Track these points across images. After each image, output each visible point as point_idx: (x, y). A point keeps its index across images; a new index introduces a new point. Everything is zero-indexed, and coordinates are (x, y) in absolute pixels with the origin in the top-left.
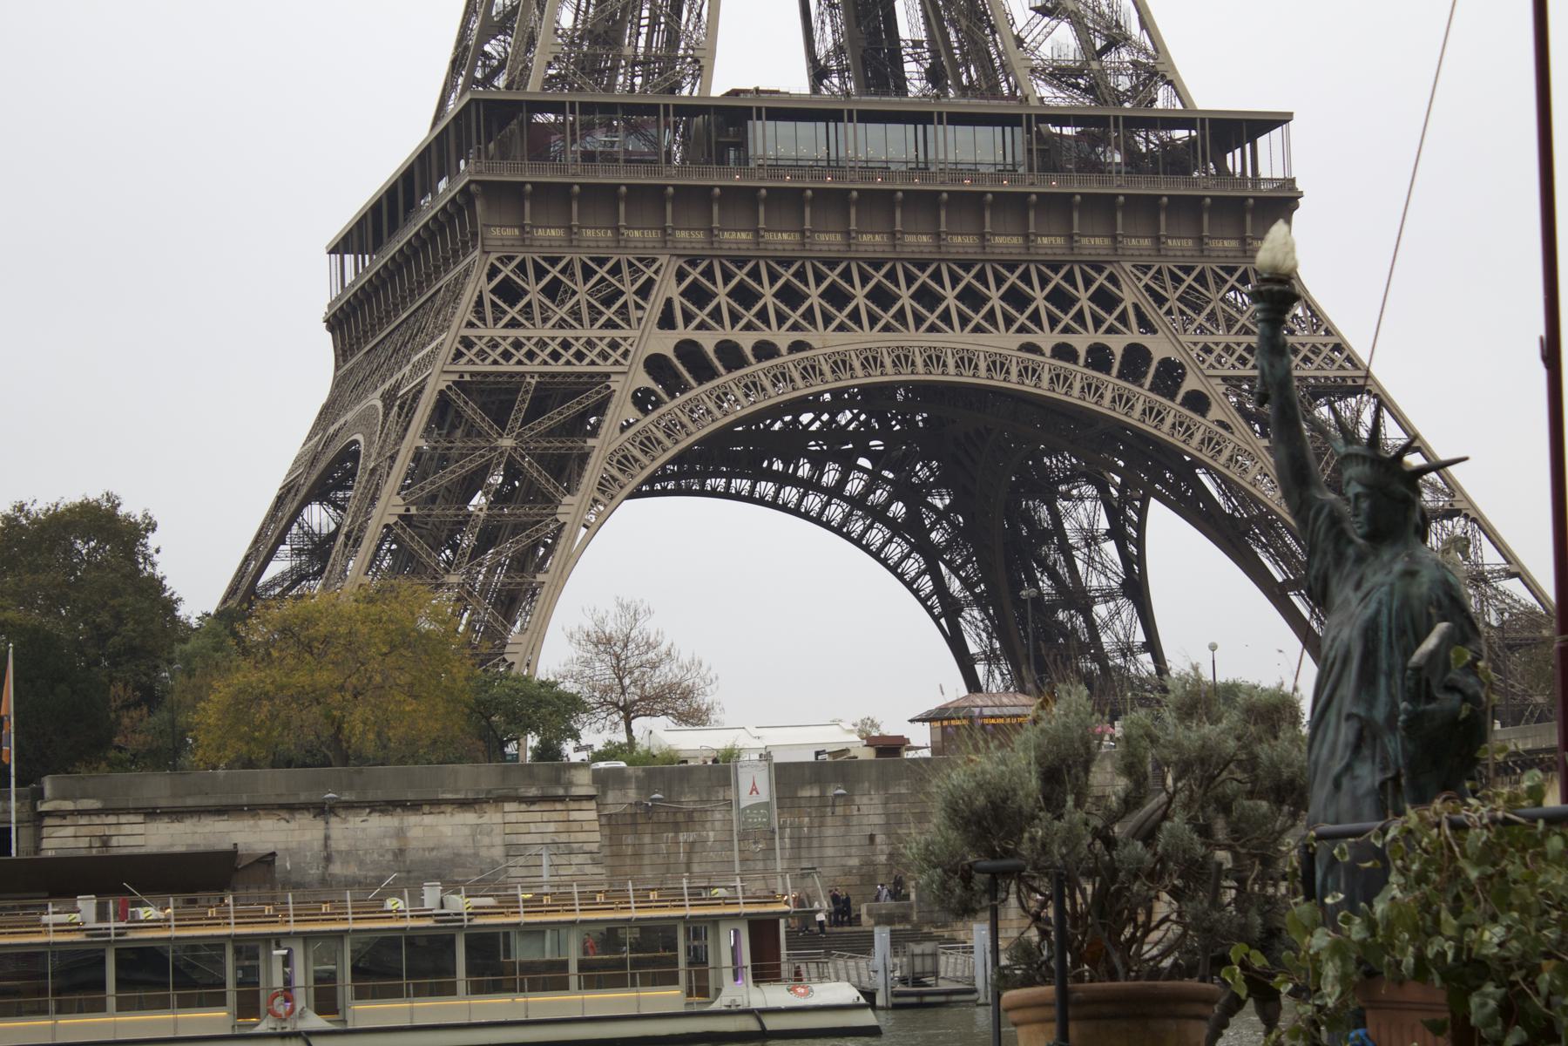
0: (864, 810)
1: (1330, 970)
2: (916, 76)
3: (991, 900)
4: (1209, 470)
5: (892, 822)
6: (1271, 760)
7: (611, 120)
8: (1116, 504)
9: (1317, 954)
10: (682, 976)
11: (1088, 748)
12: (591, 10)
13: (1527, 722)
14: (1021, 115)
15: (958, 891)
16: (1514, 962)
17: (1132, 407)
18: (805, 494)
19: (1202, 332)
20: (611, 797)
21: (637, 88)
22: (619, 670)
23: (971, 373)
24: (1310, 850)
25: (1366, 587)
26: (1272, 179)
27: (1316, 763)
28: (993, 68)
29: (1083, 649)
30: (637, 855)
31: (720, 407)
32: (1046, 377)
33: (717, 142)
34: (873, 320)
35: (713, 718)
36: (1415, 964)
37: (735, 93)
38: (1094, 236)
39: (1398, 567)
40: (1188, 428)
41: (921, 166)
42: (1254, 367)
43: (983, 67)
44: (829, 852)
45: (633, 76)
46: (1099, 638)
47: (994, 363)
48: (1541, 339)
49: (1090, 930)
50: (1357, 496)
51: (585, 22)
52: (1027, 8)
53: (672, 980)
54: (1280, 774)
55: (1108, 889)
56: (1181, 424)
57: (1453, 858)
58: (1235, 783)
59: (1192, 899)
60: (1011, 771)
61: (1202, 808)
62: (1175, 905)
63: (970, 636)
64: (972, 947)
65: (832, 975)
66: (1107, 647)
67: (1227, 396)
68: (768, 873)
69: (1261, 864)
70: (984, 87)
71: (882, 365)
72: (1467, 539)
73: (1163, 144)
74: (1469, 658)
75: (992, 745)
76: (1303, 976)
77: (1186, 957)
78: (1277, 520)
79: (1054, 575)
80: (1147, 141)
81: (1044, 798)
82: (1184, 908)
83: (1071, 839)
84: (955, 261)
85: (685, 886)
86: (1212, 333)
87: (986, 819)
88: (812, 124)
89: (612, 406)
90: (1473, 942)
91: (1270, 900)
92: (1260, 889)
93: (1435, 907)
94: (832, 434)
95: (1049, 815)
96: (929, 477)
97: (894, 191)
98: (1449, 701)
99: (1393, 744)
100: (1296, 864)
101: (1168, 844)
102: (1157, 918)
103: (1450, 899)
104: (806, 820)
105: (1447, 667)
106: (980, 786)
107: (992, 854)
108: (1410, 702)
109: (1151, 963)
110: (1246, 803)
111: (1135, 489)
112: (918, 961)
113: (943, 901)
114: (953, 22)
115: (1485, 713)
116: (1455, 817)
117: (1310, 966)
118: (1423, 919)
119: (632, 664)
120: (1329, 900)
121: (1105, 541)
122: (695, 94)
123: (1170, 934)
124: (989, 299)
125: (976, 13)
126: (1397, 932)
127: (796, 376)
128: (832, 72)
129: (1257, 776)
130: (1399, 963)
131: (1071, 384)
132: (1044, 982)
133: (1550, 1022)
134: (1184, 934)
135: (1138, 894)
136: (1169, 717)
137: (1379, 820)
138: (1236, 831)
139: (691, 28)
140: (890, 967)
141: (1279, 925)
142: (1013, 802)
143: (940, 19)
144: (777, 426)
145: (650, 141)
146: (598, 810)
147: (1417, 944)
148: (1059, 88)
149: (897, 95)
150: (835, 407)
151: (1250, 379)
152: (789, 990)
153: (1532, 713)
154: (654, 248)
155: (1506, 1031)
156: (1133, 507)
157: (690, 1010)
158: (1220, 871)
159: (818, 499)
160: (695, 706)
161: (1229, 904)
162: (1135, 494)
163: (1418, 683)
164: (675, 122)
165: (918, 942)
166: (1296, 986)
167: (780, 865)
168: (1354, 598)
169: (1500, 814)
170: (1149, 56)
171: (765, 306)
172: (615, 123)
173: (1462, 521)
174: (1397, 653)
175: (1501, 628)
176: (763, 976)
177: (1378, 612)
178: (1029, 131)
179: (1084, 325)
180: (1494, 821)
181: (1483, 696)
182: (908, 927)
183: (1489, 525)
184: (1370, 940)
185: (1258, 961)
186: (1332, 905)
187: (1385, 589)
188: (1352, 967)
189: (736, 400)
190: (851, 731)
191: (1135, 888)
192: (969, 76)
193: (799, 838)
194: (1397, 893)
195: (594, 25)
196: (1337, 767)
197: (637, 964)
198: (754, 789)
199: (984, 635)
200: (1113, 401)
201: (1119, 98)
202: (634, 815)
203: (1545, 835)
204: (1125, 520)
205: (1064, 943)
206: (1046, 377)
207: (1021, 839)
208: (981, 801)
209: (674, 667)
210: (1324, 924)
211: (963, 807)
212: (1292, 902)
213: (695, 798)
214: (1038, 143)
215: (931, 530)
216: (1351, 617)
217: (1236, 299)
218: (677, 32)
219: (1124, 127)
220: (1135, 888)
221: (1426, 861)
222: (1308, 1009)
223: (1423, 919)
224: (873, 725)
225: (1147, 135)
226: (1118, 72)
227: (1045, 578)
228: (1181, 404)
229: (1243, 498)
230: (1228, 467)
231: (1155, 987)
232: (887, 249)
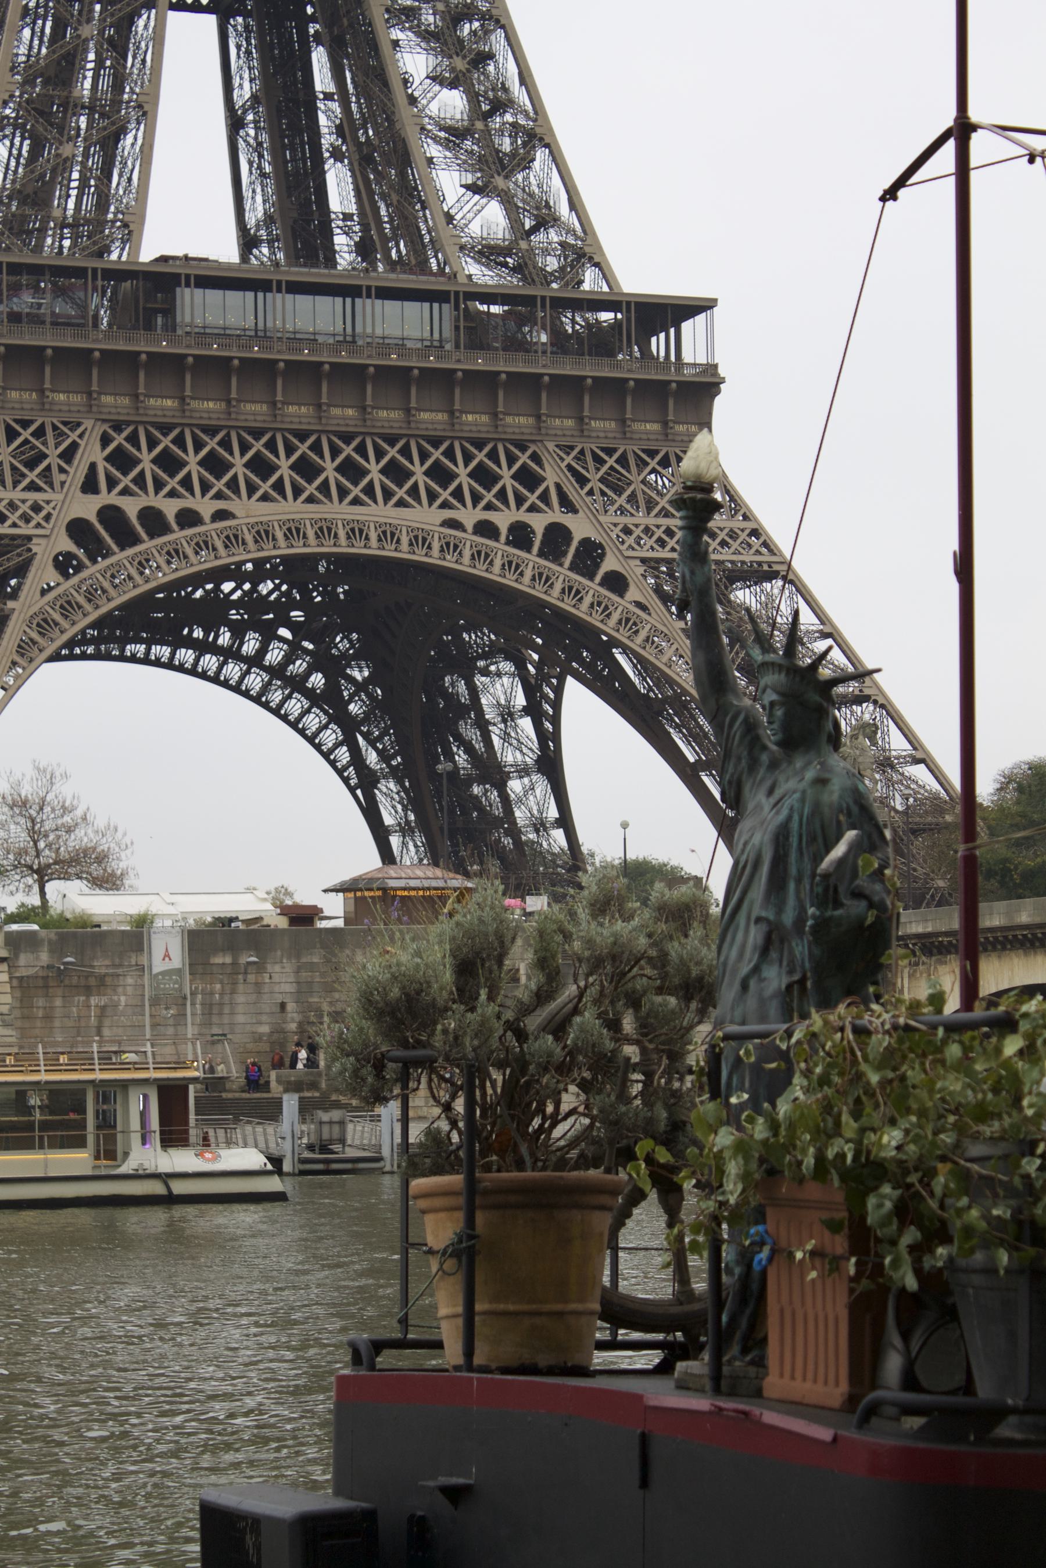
0: (276, 978)
1: (733, 1168)
2: (346, 249)
3: (402, 1089)
4: (626, 650)
5: (303, 990)
6: (681, 959)
7: (39, 282)
8: (533, 681)
9: (721, 1151)
10: (90, 1139)
11: (502, 942)
12: (20, 170)
13: (928, 906)
14: (449, 292)
15: (370, 1080)
16: (910, 1165)
17: (551, 586)
18: (225, 663)
19: (622, 513)
20: (23, 959)
21: (65, 251)
22: (34, 832)
24: (717, 1050)
25: (778, 793)
26: (695, 364)
27: (725, 964)
28: (423, 243)
29: (497, 822)
30: (48, 1017)
31: (142, 573)
32: (467, 553)
33: (144, 308)
34: (297, 491)
35: (127, 882)
36: (816, 1164)
37: (164, 259)
38: (519, 415)
39: (810, 775)
40: (606, 608)
41: (349, 339)
42: (673, 550)
43: (412, 242)
44: (240, 1019)
45: (62, 238)
46: (513, 813)
47: (416, 537)
48: (955, 553)
49: (499, 1120)
50: (772, 704)
51: (14, 182)
52: (458, 185)
53: (79, 1143)
54: (689, 971)
55: (518, 1081)
56: (599, 604)
57: (855, 1062)
58: (645, 979)
59: (600, 1092)
60: (426, 965)
62: (583, 1097)
63: (386, 808)
64: (379, 1116)
65: (240, 1141)
66: (520, 822)
67: (644, 577)
68: (178, 1040)
69: (668, 1058)
70: (413, 262)
71: (305, 537)
72: (875, 725)
73: (589, 326)
74: (876, 865)
75: (407, 937)
76: (706, 1172)
77: (592, 1148)
78: (690, 702)
79: (469, 749)
80: (574, 322)
81: (458, 990)
82: (592, 1100)
83: (483, 1031)
84: (380, 436)
85: (95, 1049)
86: (632, 515)
87: (399, 1010)
88: (240, 294)
89: (33, 570)
90: (873, 1144)
91: (676, 1094)
92: (666, 1083)
93: (836, 1109)
94: (254, 604)
95: (463, 1007)
96: (348, 650)
97: (321, 364)
98: (855, 908)
99: (800, 948)
100: (702, 1063)
101: (578, 1039)
102: (565, 1108)
103: (850, 1101)
104: (218, 986)
105: (855, 875)
106: (394, 977)
107: (405, 1045)
108: (818, 908)
109: (558, 1153)
110: (659, 999)
111: (552, 666)
112: (326, 1129)
113: (355, 1089)
114: (384, 197)
115: (890, 919)
116: (858, 1022)
117: (713, 1163)
118: (824, 1120)
119: (47, 828)
120: (733, 1100)
121: (521, 717)
122: (124, 258)
123: (577, 1126)
124: (412, 474)
125: (407, 188)
126: (799, 1133)
127: (219, 544)
128: (261, 241)
129: (667, 974)
130: (800, 1163)
131: (492, 561)
132: (452, 1171)
133: (943, 1223)
134: (591, 1126)
135: (547, 1086)
136: (583, 914)
137: (785, 1022)
138: (644, 1026)
139: (121, 192)
140: (298, 1134)
141: (684, 1118)
142: (427, 994)
143: (371, 193)
144: (199, 594)
145: (77, 304)
146: (10, 972)
147: (818, 1145)
148: (487, 266)
149: (326, 267)
150: (256, 578)
151: (668, 562)
152: (196, 1155)
153: (933, 896)
154: (79, 411)
155: (901, 1231)
156: (550, 685)
157: (97, 1173)
158: (629, 1066)
159: (237, 668)
160: (109, 870)
161: (636, 1097)
162: (553, 672)
163: (826, 890)
164: (103, 286)
165: (326, 1110)
167: (190, 1031)
168: (767, 804)
169: (902, 1021)
170: (577, 238)
171: (189, 474)
172: (42, 285)
173: (871, 707)
174: (806, 859)
175: (905, 813)
176: (171, 1140)
177: (789, 818)
178: (457, 308)
179: (506, 502)
180: (895, 1027)
181: (889, 903)
182: (317, 1094)
183: (897, 712)
184: (772, 1140)
185: (663, 1156)
186: (736, 1105)
187: (797, 796)
188: (754, 1166)
189: (158, 567)
190: (265, 900)
191: (545, 1080)
192: (399, 251)
193: (211, 1005)
194: (799, 1094)
195: (22, 185)
196: (745, 969)
197: (45, 1126)
198: (167, 955)
199: (399, 807)
200: (533, 579)
201: (546, 278)
202: (45, 978)
203: (945, 1042)
204: (541, 697)
205: (472, 1132)
206: (467, 553)
207: (434, 1031)
208: (395, 992)
209: (90, 831)
210: (728, 1123)
211: (378, 998)
212: (697, 1100)
213: (107, 962)
214: (465, 320)
215: (350, 701)
217: (656, 482)
218: (107, 196)
219: (551, 308)
220: (545, 1080)
221: (829, 1065)
222: (710, 1205)
223: (824, 1120)
224: (288, 893)
225: (573, 316)
226: (546, 252)
227: (461, 753)
228: (599, 584)
229: (658, 678)
230: (644, 648)
231: (561, 1178)
232: (312, 421)
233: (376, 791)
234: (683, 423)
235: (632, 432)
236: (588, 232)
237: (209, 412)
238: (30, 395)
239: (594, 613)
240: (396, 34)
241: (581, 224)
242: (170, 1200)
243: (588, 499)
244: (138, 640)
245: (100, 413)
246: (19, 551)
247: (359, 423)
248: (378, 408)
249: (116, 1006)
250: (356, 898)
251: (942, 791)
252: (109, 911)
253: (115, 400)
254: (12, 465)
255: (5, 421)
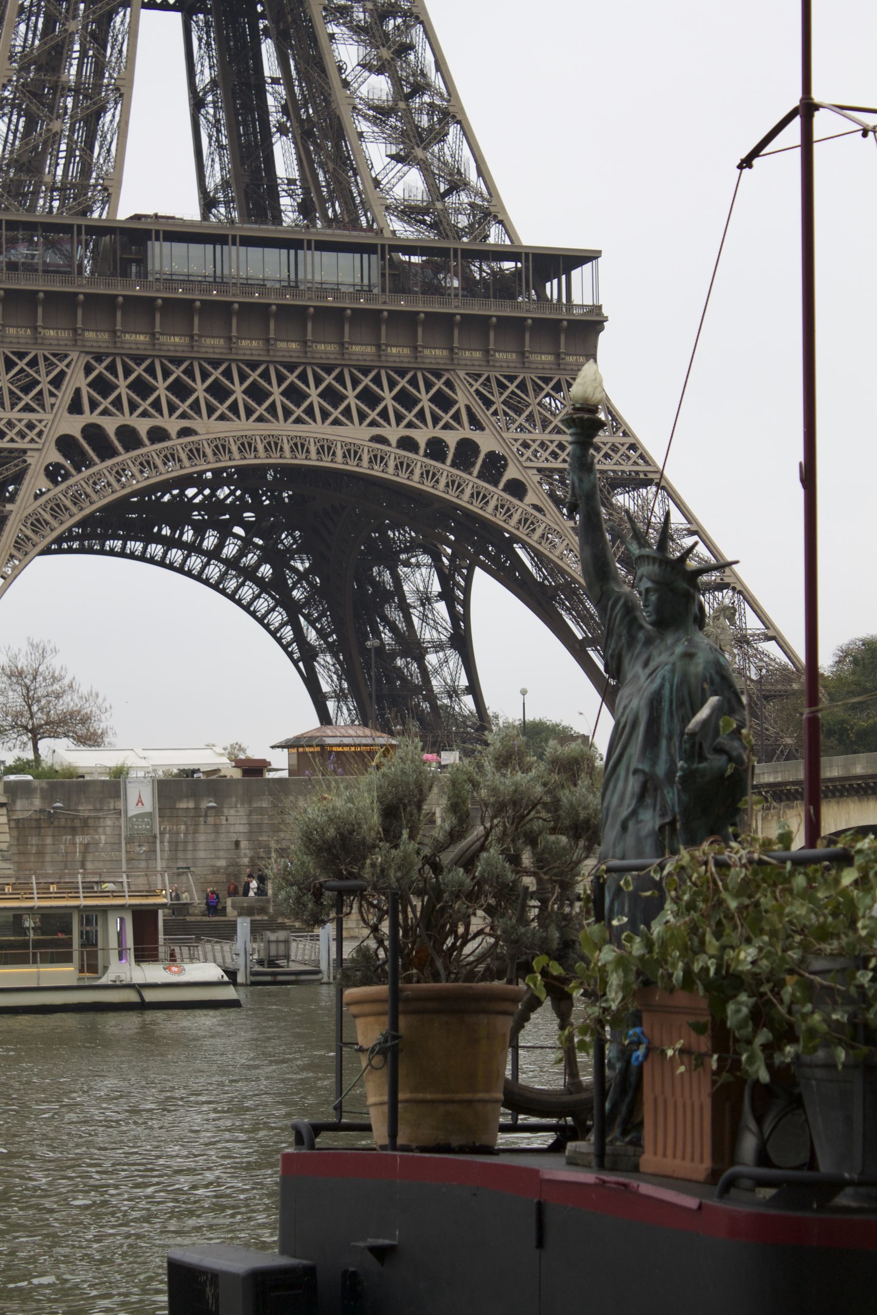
0: (232, 820)
1: (614, 980)
2: (290, 209)
3: (337, 914)
4: (525, 545)
5: (254, 830)
6: (571, 804)
7: (33, 236)
8: (447, 571)
9: (604, 966)
10: (76, 956)
11: (421, 790)
12: (17, 143)
13: (778, 759)
14: (376, 245)
15: (310, 905)
16: (763, 977)
17: (462, 491)
18: (189, 556)
19: (521, 430)
20: (20, 804)
21: (55, 210)
22: (29, 698)
23: (278, 454)
24: (601, 881)
25: (652, 665)
26: (583, 306)
27: (608, 808)
28: (354, 204)
29: (417, 689)
30: (41, 853)
31: (119, 481)
32: (392, 464)
33: (121, 259)
34: (249, 412)
35: (106, 740)
36: (684, 976)
37: (137, 217)
38: (435, 348)
39: (679, 650)
40: (508, 510)
41: (292, 284)
42: (564, 461)
43: (346, 203)
44: (202, 854)
45: (52, 200)
46: (430, 682)
47: (349, 451)
48: (800, 464)
49: (418, 940)
51: (11, 152)
52: (384, 155)
53: (66, 958)
54: (578, 814)
55: (434, 906)
56: (502, 507)
57: (717, 890)
58: (540, 821)
59: (503, 915)
60: (357, 809)
61: (513, 841)
62: (489, 920)
63: (323, 678)
64: (318, 936)
65: (201, 957)
66: (436, 690)
67: (540, 484)
68: (149, 872)
69: (560, 887)
70: (347, 220)
71: (256, 450)
72: (734, 608)
73: (494, 273)
74: (735, 726)
78: (579, 588)
79: (393, 628)
80: (481, 270)
81: (384, 830)
82: (496, 923)
83: (405, 865)
84: (319, 365)
85: (80, 880)
86: (530, 432)
87: (335, 847)
88: (201, 246)
89: (28, 478)
90: (732, 960)
91: (567, 918)
92: (559, 908)
93: (701, 930)
94: (213, 506)
95: (388, 845)
96: (292, 545)
97: (269, 305)
98: (717, 761)
99: (671, 795)
100: (589, 892)
101: (484, 871)
102: (473, 929)
103: (713, 923)
104: (183, 827)
105: (717, 733)
106: (331, 820)
107: (339, 876)
108: (686, 762)
110: (552, 838)
111: (463, 559)
112: (273, 947)
113: (297, 913)
114: (322, 165)
115: (746, 770)
116: (719, 857)
117: (598, 975)
118: (691, 939)
119: (40, 694)
120: (615, 923)
121: (437, 601)
122: (104, 217)
123: (484, 944)
124: (346, 397)
125: (341, 157)
126: (670, 950)
127: (184, 456)
128: (219, 202)
129: (559, 817)
130: (670, 976)
131: (412, 470)
132: (379, 982)
133: (791, 1026)
134: (496, 944)
135: (459, 911)
136: (489, 767)
137: (658, 857)
138: (540, 861)
139: (101, 161)
140: (250, 951)
141: (573, 938)
142: (358, 834)
143: (311, 162)
144: (167, 498)
145: (64, 255)
146: (8, 816)
147: (686, 960)
148: (408, 223)
149: (273, 224)
150: (215, 485)
151: (560, 471)
152: (165, 969)
153: (782, 751)
154: (66, 345)
156: (461, 574)
157: (81, 983)
158: (527, 894)
159: (199, 560)
160: (92, 730)
161: (533, 920)
162: (464, 564)
163: (693, 746)
164: (86, 240)
165: (273, 930)
166: (586, 991)
167: (160, 865)
168: (643, 674)
169: (756, 856)
170: (484, 199)
171: (158, 398)
172: (36, 239)
173: (730, 593)
174: (676, 721)
175: (759, 682)
176: (143, 956)
177: (662, 686)
178: (383, 258)
179: (424, 421)
180: (751, 861)
181: (745, 757)
182: (266, 918)
183: (752, 597)
184: (647, 956)
185: (556, 970)
186: (617, 927)
187: (668, 667)
188: (632, 977)
189: (133, 476)
190: (222, 755)
191: (457, 906)
192: (334, 211)
193: (177, 843)
194: (670, 917)
195: (19, 155)
196: (625, 813)
197: (37, 944)
198: (140, 801)
199: (335, 677)
200: (447, 485)
201: (458, 233)
202: (38, 820)
203: (792, 874)
204: (454, 584)
205: (396, 949)
206: (392, 464)
207: (364, 864)
208: (331, 832)
209: (75, 697)
210: (610, 942)
211: (317, 837)
212: (585, 922)
213: (90, 807)
214: (390, 268)
215: (293, 588)
216: (639, 690)
217: (550, 404)
218: (90, 164)
219: (462, 258)
220: (457, 906)
221: (695, 893)
222: (596, 1011)
223: (691, 939)
224: (241, 749)
225: (481, 265)
226: (458, 211)
227: (386, 631)
228: (503, 490)
229: (552, 569)
230: (540, 543)
231: (470, 988)
232: (262, 353)
233: (316, 664)
234: (573, 355)
235: (530, 362)
236: (493, 194)
237: (175, 346)
238: (25, 332)
239: (498, 514)
240: (332, 28)
241: (487, 188)
242: (143, 1006)
243: (493, 419)
244: (116, 537)
245: (84, 346)
246: (16, 462)
247: (301, 355)
248: (317, 342)
249: (97, 843)
250: (298, 753)
251: (790, 664)
252: (92, 764)
253: (97, 336)
254: (10, 390)
255: (4, 353)
